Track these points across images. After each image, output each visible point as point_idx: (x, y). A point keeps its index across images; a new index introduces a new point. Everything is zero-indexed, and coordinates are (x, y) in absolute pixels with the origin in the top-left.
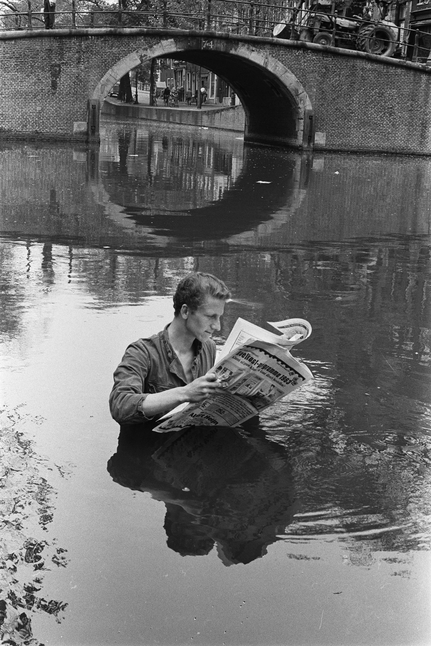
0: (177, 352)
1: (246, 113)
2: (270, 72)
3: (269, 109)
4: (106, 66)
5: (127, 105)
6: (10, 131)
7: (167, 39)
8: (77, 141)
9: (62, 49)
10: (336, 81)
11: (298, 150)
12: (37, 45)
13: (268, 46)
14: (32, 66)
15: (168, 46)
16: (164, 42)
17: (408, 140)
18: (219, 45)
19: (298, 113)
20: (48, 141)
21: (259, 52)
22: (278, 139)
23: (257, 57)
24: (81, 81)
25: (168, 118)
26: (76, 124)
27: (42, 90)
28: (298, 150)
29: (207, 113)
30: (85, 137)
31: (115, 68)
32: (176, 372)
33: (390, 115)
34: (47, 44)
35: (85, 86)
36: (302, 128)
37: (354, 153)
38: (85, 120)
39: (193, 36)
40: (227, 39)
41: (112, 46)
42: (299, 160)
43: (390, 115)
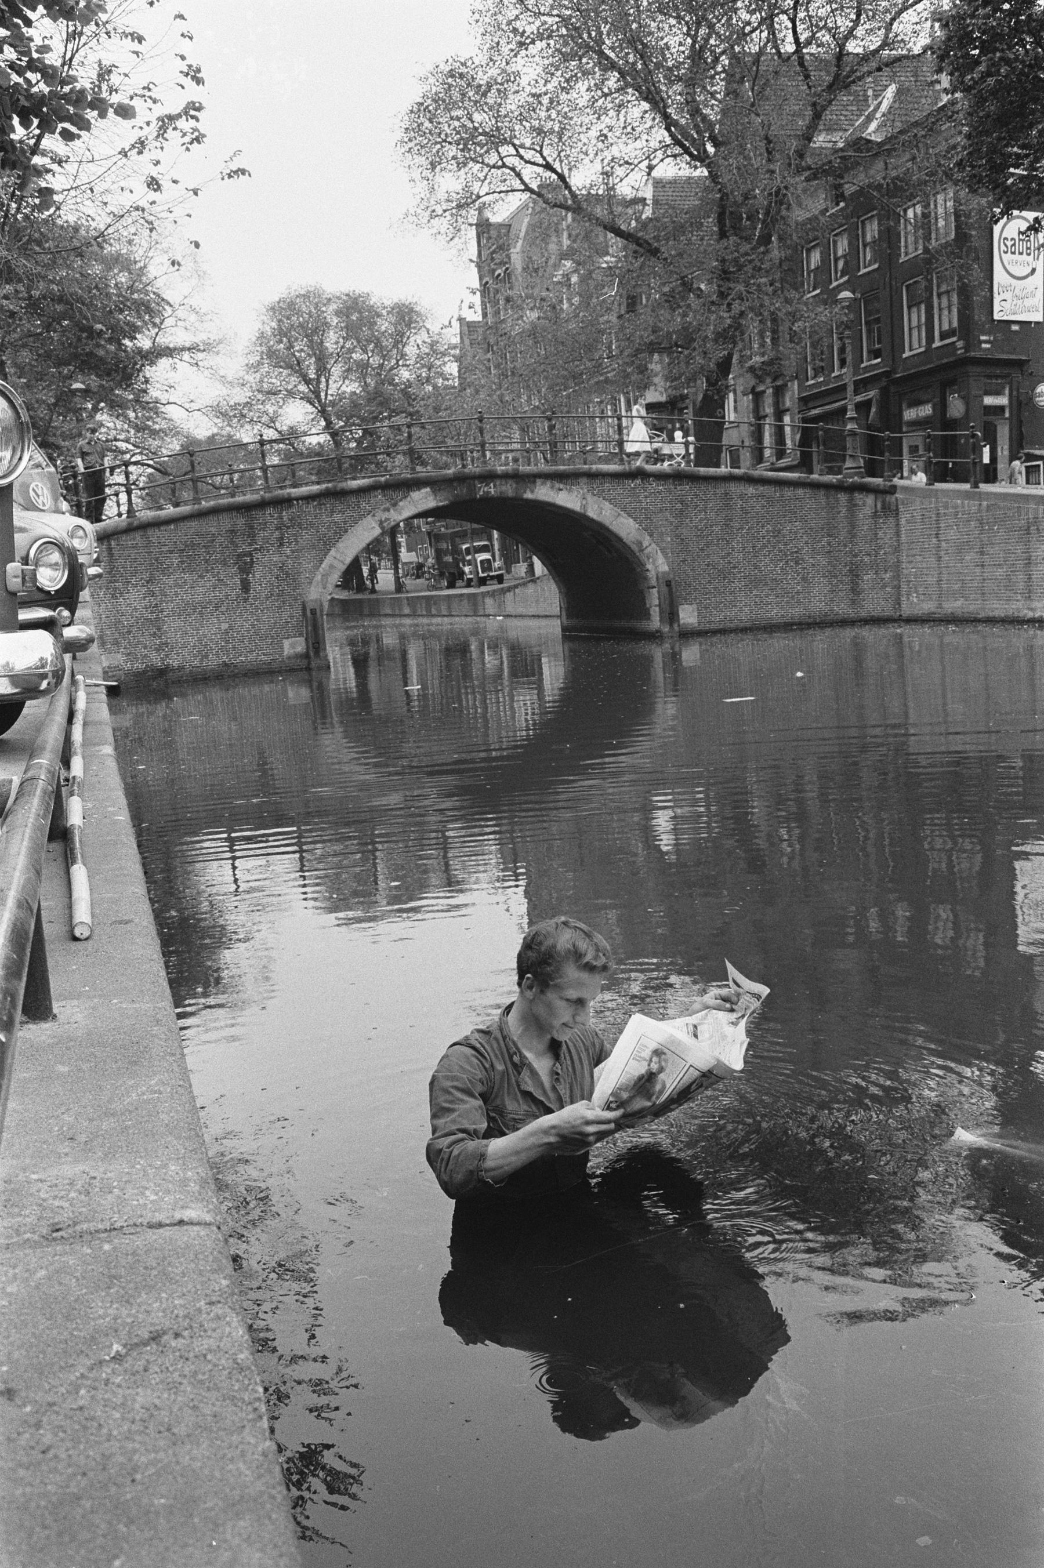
0: (529, 1055)
1: (559, 588)
2: (592, 520)
3: (597, 578)
4: (326, 544)
5: (360, 596)
6: (181, 668)
7: (419, 489)
8: (291, 670)
9: (252, 528)
10: (701, 521)
11: (655, 637)
12: (211, 526)
13: (583, 480)
14: (206, 561)
15: (423, 500)
16: (416, 495)
17: (832, 600)
18: (504, 488)
19: (646, 578)
20: (245, 675)
21: (570, 491)
22: (623, 623)
23: (568, 499)
24: (287, 574)
25: (429, 610)
26: (286, 643)
27: (227, 596)
28: (655, 637)
29: (492, 594)
30: (305, 662)
31: (340, 545)
32: (531, 1089)
33: (797, 563)
34: (226, 522)
35: (294, 580)
36: (657, 602)
37: (744, 630)
38: (301, 635)
39: (461, 479)
40: (515, 476)
41: (332, 512)
42: (658, 653)
43: (797, 563)
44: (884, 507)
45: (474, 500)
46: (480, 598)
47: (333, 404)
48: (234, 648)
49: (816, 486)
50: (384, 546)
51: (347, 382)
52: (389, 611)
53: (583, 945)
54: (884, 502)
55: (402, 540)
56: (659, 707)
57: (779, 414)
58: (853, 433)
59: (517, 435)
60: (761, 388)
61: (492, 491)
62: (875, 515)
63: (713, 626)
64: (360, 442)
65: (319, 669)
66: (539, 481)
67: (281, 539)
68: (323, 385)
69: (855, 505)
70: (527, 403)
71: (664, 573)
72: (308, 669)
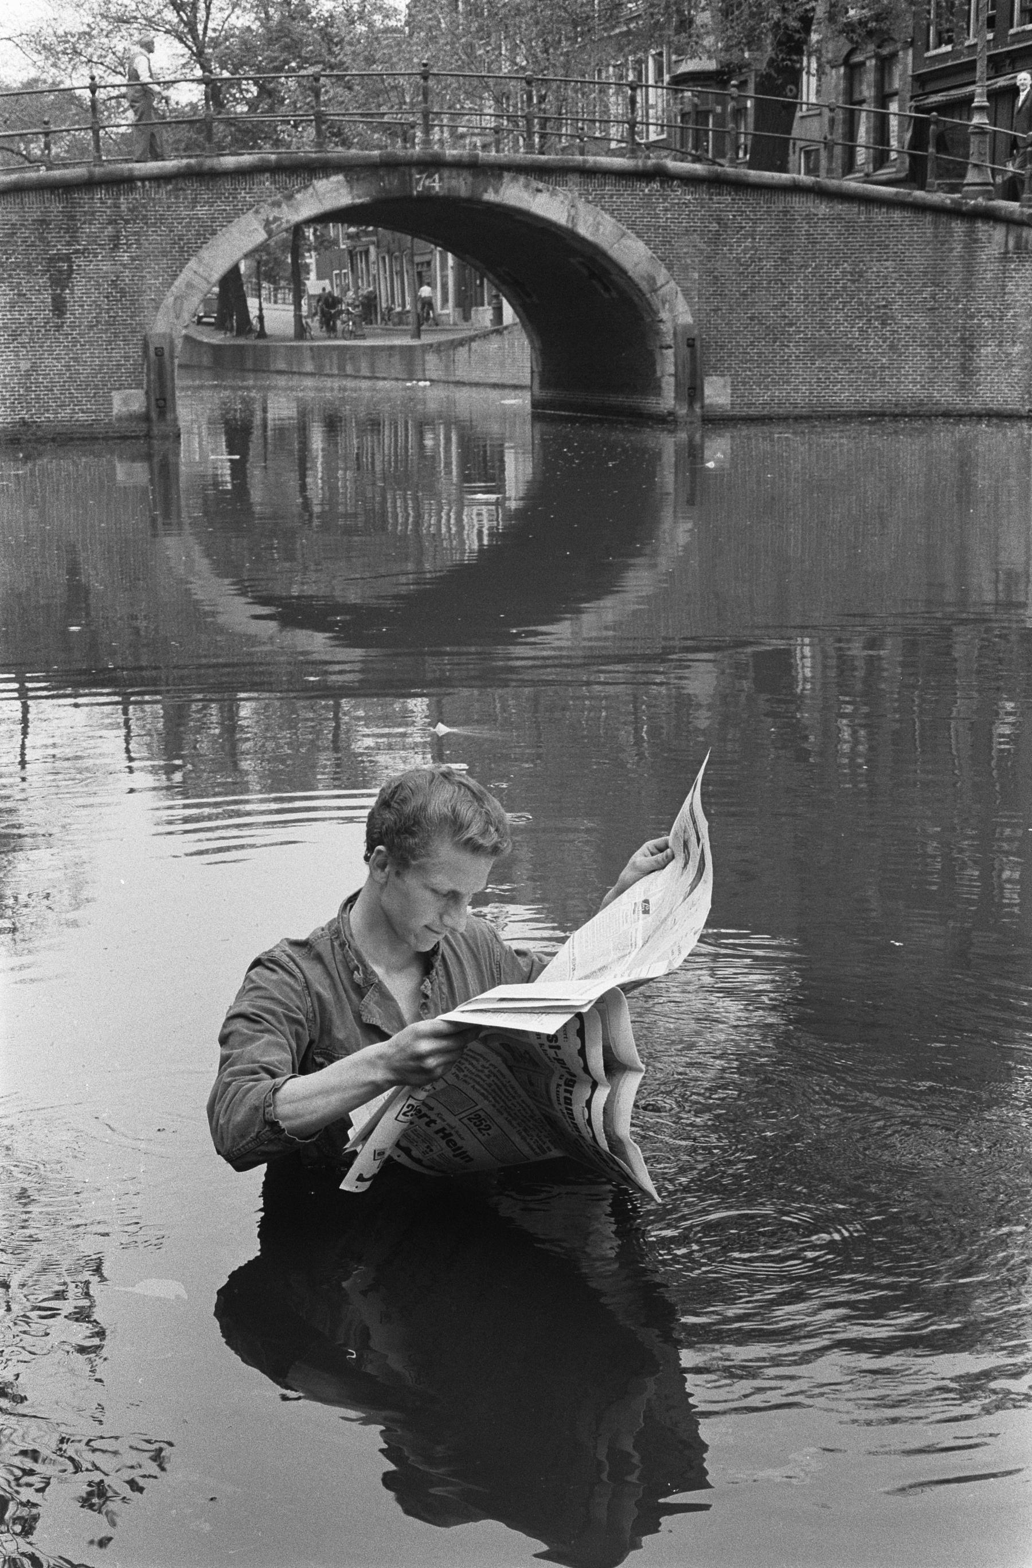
0: (379, 970)
1: (531, 342)
2: (583, 240)
3: (586, 326)
4: (184, 249)
5: (241, 341)
7: (327, 177)
9: (72, 218)
11: (666, 421)
13: (574, 179)
15: (332, 193)
16: (321, 185)
18: (454, 182)
19: (658, 333)
21: (554, 193)
22: (619, 399)
23: (549, 205)
24: (123, 292)
25: (342, 368)
26: (117, 397)
28: (666, 421)
29: (437, 348)
30: (144, 426)
31: (204, 253)
33: (884, 324)
34: (33, 207)
35: (133, 302)
36: (671, 369)
38: (139, 386)
39: (390, 165)
41: (195, 202)
42: (668, 445)
43: (884, 324)
44: (1018, 246)
45: (409, 199)
46: (419, 353)
47: (215, 43)
48: (38, 398)
49: (921, 208)
50: (279, 263)
51: (238, 11)
52: (282, 366)
53: (466, 811)
54: (1019, 238)
55: (311, 259)
56: (666, 525)
57: (883, 98)
58: (981, 131)
59: (489, 106)
60: (857, 58)
61: (437, 186)
62: (1005, 257)
63: (752, 411)
64: (253, 105)
65: (165, 437)
66: (507, 176)
67: (115, 239)
68: (201, 14)
69: (976, 241)
70: (509, 59)
71: (687, 327)
72: (148, 436)
